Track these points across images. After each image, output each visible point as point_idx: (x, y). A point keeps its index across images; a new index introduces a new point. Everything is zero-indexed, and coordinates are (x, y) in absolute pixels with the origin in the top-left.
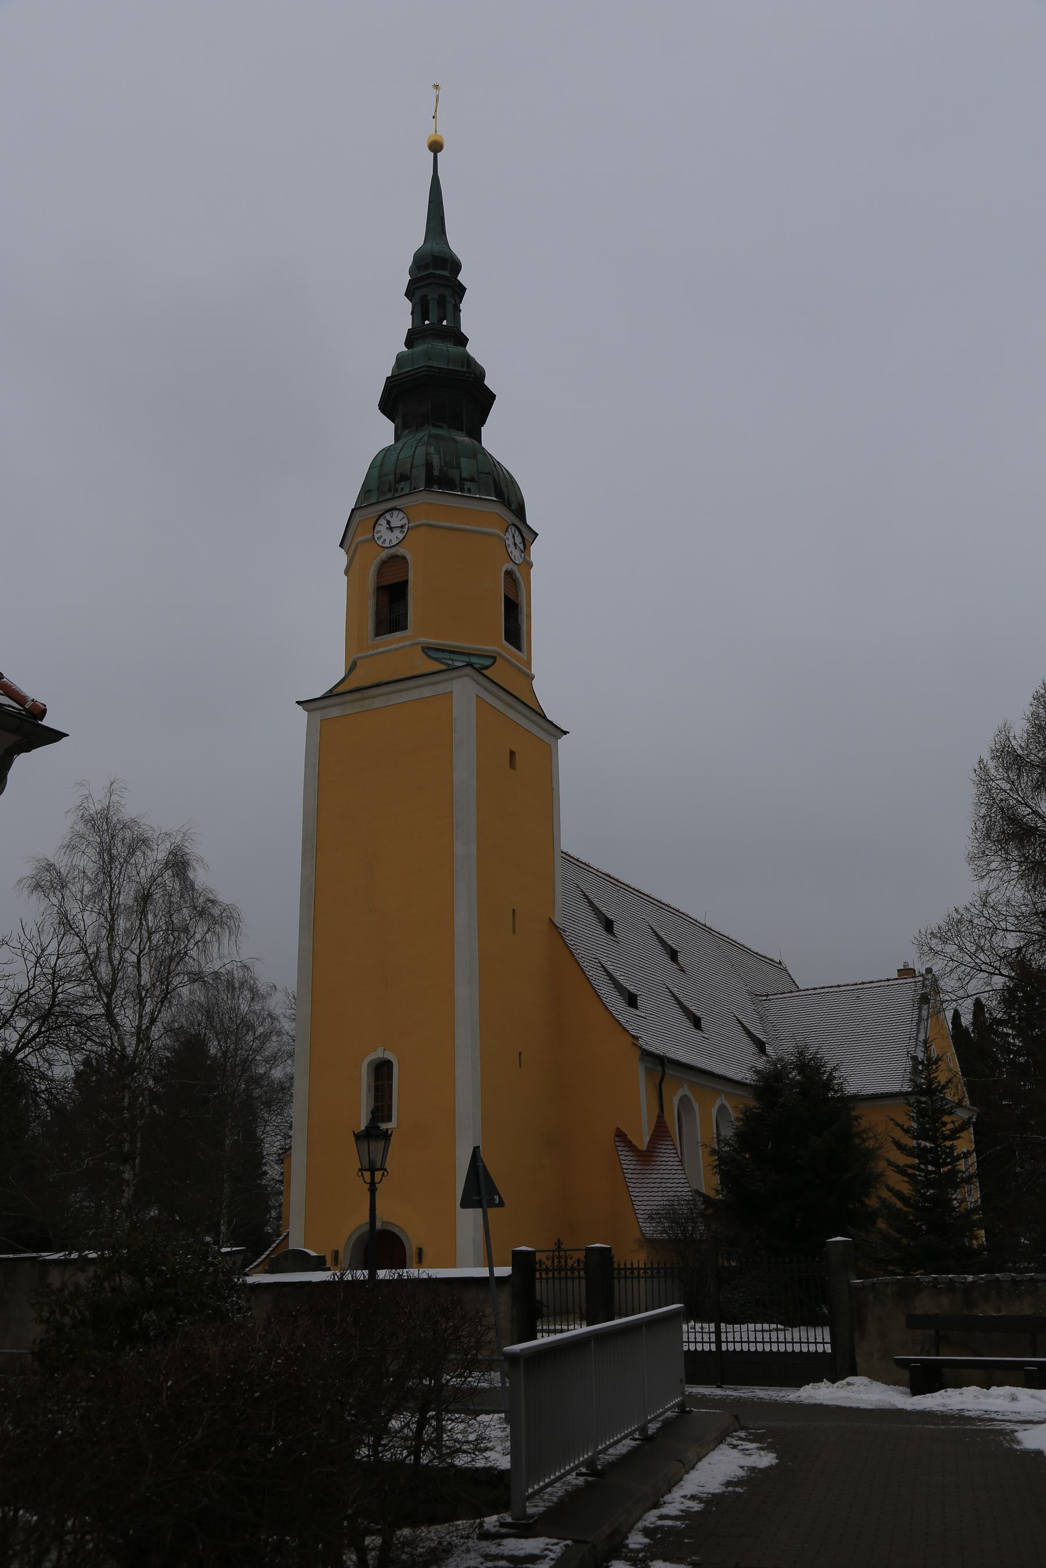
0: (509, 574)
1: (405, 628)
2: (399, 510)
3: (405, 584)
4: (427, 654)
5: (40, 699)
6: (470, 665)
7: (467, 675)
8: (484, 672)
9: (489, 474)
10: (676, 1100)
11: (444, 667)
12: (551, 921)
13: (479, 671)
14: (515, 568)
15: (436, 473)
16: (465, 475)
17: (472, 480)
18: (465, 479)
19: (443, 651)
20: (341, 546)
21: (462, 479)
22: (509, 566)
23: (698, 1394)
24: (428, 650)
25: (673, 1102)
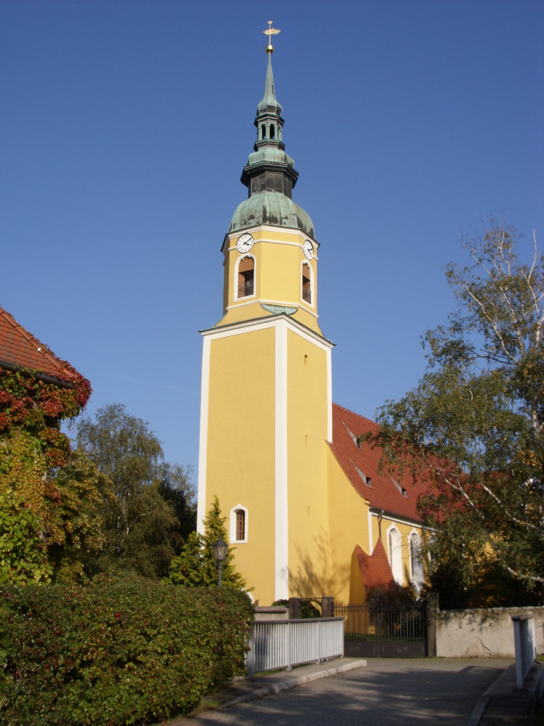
0: (305, 265)
1: (253, 294)
2: (250, 234)
3: (252, 271)
4: (263, 307)
5: (210, 341)
6: (284, 313)
7: (282, 318)
8: (291, 316)
9: (295, 214)
10: (388, 531)
11: (271, 314)
12: (326, 441)
13: (288, 316)
14: (308, 262)
15: (268, 215)
16: (282, 216)
17: (286, 218)
18: (283, 218)
19: (271, 305)
20: (222, 251)
21: (281, 218)
22: (305, 261)
23: (407, 695)
24: (312, 230)
25: (387, 532)
